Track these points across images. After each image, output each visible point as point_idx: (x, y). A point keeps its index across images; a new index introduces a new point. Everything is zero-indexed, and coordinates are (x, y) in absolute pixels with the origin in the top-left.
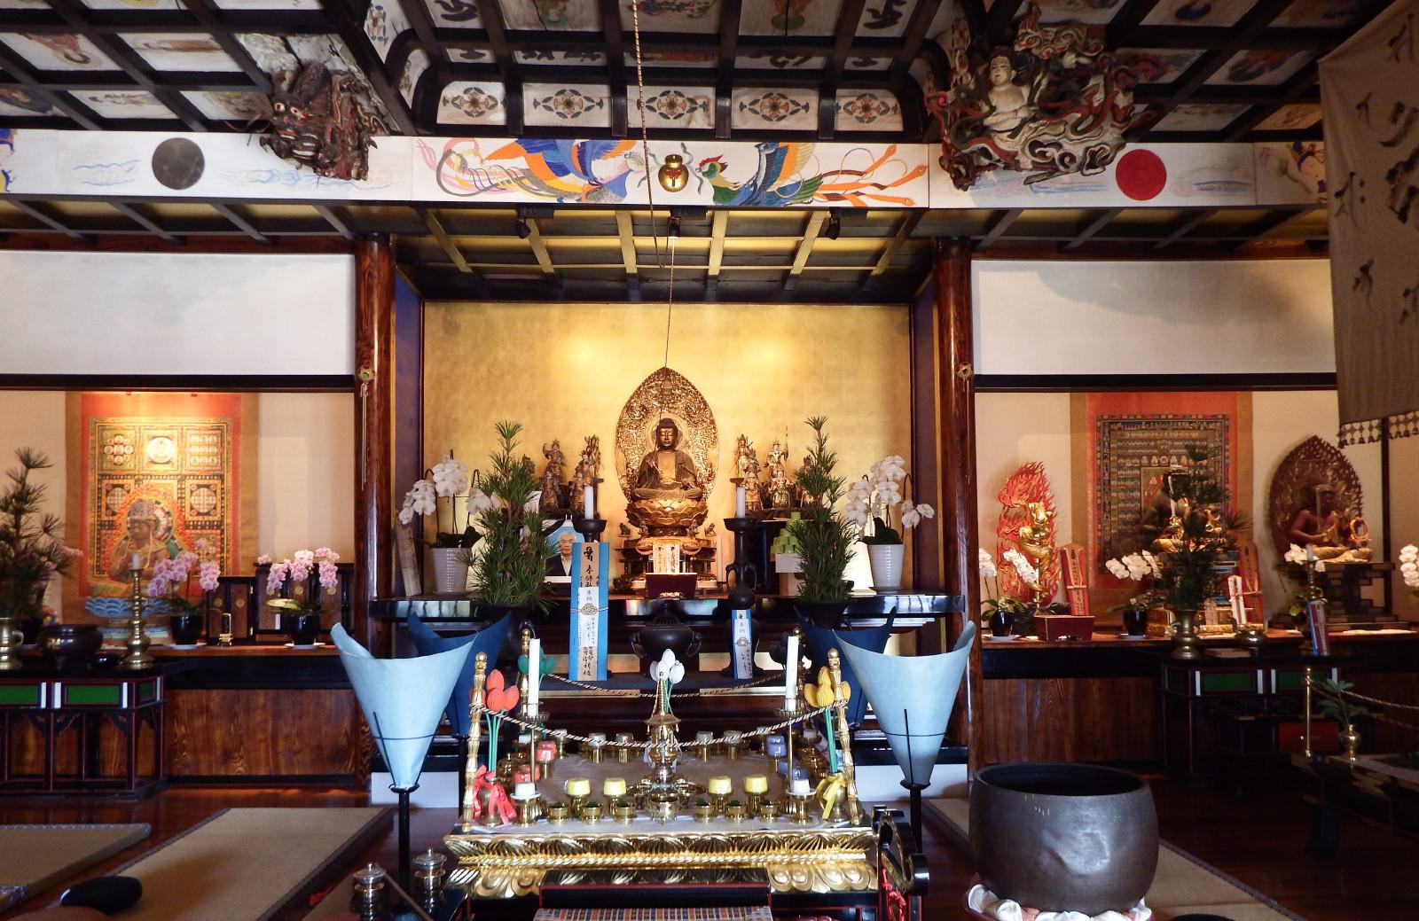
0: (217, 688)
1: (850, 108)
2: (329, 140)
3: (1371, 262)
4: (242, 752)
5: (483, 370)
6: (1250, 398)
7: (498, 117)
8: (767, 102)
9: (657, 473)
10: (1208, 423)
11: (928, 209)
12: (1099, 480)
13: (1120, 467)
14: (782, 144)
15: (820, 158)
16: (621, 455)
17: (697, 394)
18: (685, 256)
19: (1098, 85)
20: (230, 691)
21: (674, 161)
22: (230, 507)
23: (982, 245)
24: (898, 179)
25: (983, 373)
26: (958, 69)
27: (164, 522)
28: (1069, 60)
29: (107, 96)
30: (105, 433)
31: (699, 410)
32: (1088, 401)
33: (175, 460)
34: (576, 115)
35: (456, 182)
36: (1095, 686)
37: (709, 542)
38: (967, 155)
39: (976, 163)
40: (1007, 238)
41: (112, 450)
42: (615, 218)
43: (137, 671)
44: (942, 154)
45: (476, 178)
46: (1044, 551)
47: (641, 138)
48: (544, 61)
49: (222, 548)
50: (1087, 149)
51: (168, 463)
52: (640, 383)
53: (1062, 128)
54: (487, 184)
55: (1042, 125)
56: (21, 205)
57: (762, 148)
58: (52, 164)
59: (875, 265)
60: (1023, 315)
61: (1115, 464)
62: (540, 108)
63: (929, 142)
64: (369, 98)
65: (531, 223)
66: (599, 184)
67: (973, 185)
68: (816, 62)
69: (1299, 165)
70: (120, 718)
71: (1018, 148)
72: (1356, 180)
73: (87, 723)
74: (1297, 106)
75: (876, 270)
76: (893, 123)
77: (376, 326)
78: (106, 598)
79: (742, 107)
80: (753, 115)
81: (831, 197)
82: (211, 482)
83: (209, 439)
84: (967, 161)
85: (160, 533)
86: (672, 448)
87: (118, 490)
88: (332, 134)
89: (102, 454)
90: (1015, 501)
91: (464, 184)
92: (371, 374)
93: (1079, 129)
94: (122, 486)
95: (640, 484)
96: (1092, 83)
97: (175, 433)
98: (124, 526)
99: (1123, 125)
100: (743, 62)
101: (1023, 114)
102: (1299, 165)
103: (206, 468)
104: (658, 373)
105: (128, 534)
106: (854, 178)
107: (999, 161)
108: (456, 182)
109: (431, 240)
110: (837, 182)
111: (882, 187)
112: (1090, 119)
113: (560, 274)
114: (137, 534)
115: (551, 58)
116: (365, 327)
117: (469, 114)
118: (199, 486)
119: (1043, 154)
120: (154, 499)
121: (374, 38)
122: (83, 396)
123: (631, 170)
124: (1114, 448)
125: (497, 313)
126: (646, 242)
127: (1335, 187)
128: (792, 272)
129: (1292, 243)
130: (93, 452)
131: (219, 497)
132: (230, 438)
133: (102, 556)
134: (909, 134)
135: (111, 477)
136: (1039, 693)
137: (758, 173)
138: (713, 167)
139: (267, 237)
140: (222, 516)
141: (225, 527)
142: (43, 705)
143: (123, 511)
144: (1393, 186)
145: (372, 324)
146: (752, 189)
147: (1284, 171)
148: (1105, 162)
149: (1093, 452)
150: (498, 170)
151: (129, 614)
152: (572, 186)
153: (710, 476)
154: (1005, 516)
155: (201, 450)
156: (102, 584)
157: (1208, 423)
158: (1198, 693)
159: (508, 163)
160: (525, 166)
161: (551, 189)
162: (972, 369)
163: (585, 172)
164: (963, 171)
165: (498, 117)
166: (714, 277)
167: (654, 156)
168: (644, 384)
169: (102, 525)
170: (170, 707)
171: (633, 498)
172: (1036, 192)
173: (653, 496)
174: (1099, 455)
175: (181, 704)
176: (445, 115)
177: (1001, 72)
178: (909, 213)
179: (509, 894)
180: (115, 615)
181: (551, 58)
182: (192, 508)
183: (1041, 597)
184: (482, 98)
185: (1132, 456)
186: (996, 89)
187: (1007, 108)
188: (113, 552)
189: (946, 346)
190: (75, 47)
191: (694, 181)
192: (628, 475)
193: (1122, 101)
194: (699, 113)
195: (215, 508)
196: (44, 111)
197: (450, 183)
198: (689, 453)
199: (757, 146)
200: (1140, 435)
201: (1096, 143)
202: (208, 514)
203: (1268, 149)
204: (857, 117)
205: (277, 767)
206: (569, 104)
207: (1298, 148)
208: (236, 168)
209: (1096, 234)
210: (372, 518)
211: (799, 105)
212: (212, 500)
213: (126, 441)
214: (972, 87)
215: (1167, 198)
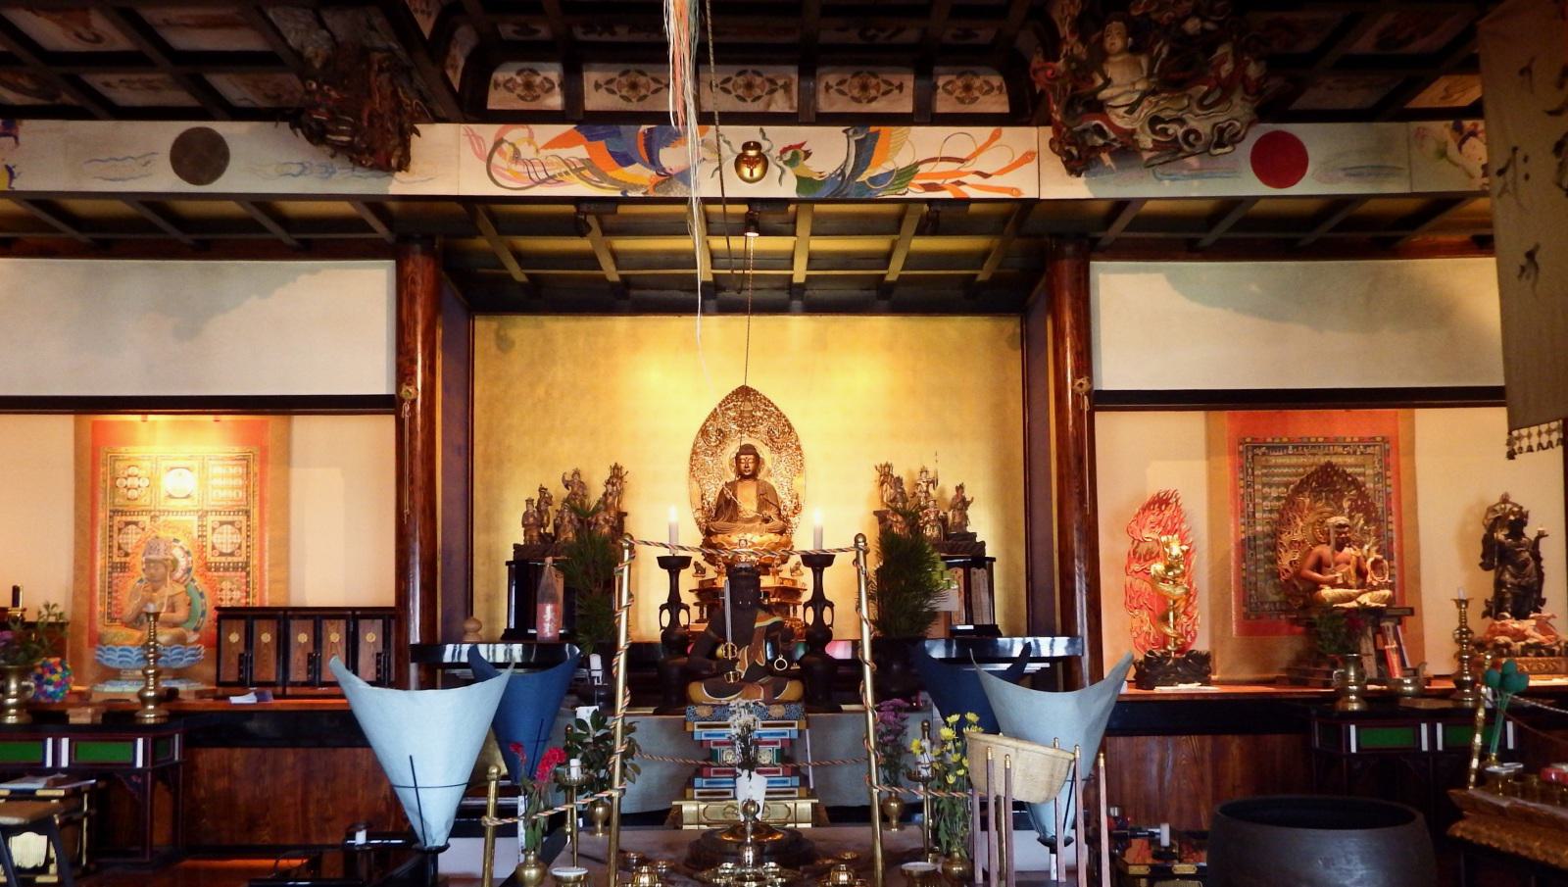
0: (242, 746)
1: (949, 87)
2: (366, 124)
3: (1537, 247)
4: (268, 818)
5: (541, 391)
6: (1413, 416)
7: (555, 101)
9: (735, 503)
10: (1365, 447)
11: (1037, 201)
13: (1265, 498)
14: (873, 129)
16: (695, 485)
17: (781, 416)
18: (766, 260)
19: (1226, 54)
20: (254, 750)
21: (752, 149)
22: (257, 546)
23: (1103, 243)
24: (1005, 166)
25: (1104, 389)
26: (1068, 39)
27: (183, 563)
28: (1192, 26)
29: (121, 81)
30: (117, 463)
31: (783, 434)
32: (1223, 418)
34: (642, 98)
35: (508, 174)
36: (1235, 745)
37: (794, 582)
39: (1090, 144)
40: (1131, 234)
41: (125, 483)
43: (150, 725)
44: (1052, 136)
45: (531, 169)
46: (1179, 591)
47: (714, 124)
48: (606, 37)
49: (248, 593)
50: (1215, 125)
51: (188, 497)
53: (1186, 102)
54: (543, 176)
55: (1164, 99)
57: (851, 133)
58: (57, 160)
59: (981, 268)
60: (1150, 322)
62: (603, 91)
63: (1038, 125)
64: (411, 80)
65: (592, 220)
68: (911, 35)
69: (1460, 149)
70: (134, 779)
71: (1137, 126)
72: (1520, 155)
74: (1458, 77)
76: (998, 104)
77: (419, 338)
78: (117, 645)
79: (828, 88)
80: (841, 97)
81: (928, 187)
82: (236, 518)
83: (233, 470)
84: (1077, 139)
85: (178, 575)
88: (370, 115)
89: (114, 487)
90: (1146, 534)
91: (516, 176)
93: (1206, 103)
94: (136, 523)
95: (717, 517)
96: (1220, 51)
97: (195, 464)
98: (140, 567)
100: (829, 36)
101: (1140, 86)
102: (1460, 149)
103: (230, 503)
105: (144, 576)
106: (954, 166)
107: (1114, 140)
108: (508, 174)
109: (481, 243)
110: (935, 171)
111: (985, 176)
112: (1217, 94)
114: (152, 576)
115: (613, 33)
116: (407, 339)
117: (522, 98)
118: (222, 523)
119: (1164, 131)
120: (171, 536)
121: (416, 10)
122: (95, 423)
124: (1258, 476)
126: (719, 243)
127: (1496, 167)
129: (1457, 238)
130: (103, 484)
132: (256, 469)
133: (114, 602)
134: (1016, 117)
135: (123, 513)
137: (846, 161)
138: (795, 156)
139: (297, 240)
140: (248, 557)
143: (137, 550)
144: (1560, 160)
145: (415, 335)
146: (840, 179)
147: (1443, 154)
148: (1235, 140)
150: (555, 160)
151: (143, 665)
152: (638, 177)
154: (1135, 552)
155: (225, 482)
156: (113, 630)
157: (1365, 447)
158: (1354, 750)
159: (565, 153)
160: (585, 155)
161: (614, 182)
163: (653, 161)
164: (1075, 152)
165: (555, 101)
167: (728, 143)
169: (113, 567)
170: (189, 764)
171: (708, 533)
174: (1242, 483)
175: (200, 766)
176: (496, 100)
177: (1115, 39)
180: (128, 666)
181: (613, 33)
182: (214, 548)
183: (1176, 644)
184: (538, 80)
186: (1112, 59)
187: (1122, 86)
188: (128, 595)
189: (1061, 365)
190: (87, 25)
191: (774, 171)
192: (703, 508)
193: (1253, 70)
194: (779, 95)
195: (240, 548)
197: (503, 176)
198: (772, 481)
199: (845, 131)
200: (1287, 460)
201: (1225, 118)
202: (232, 554)
203: (1424, 129)
204: (958, 98)
205: (307, 835)
206: (634, 86)
207: (1458, 128)
208: (263, 164)
210: (414, 553)
211: (890, 84)
212: (238, 539)
213: (142, 473)
214: (1084, 57)
215: (1309, 186)
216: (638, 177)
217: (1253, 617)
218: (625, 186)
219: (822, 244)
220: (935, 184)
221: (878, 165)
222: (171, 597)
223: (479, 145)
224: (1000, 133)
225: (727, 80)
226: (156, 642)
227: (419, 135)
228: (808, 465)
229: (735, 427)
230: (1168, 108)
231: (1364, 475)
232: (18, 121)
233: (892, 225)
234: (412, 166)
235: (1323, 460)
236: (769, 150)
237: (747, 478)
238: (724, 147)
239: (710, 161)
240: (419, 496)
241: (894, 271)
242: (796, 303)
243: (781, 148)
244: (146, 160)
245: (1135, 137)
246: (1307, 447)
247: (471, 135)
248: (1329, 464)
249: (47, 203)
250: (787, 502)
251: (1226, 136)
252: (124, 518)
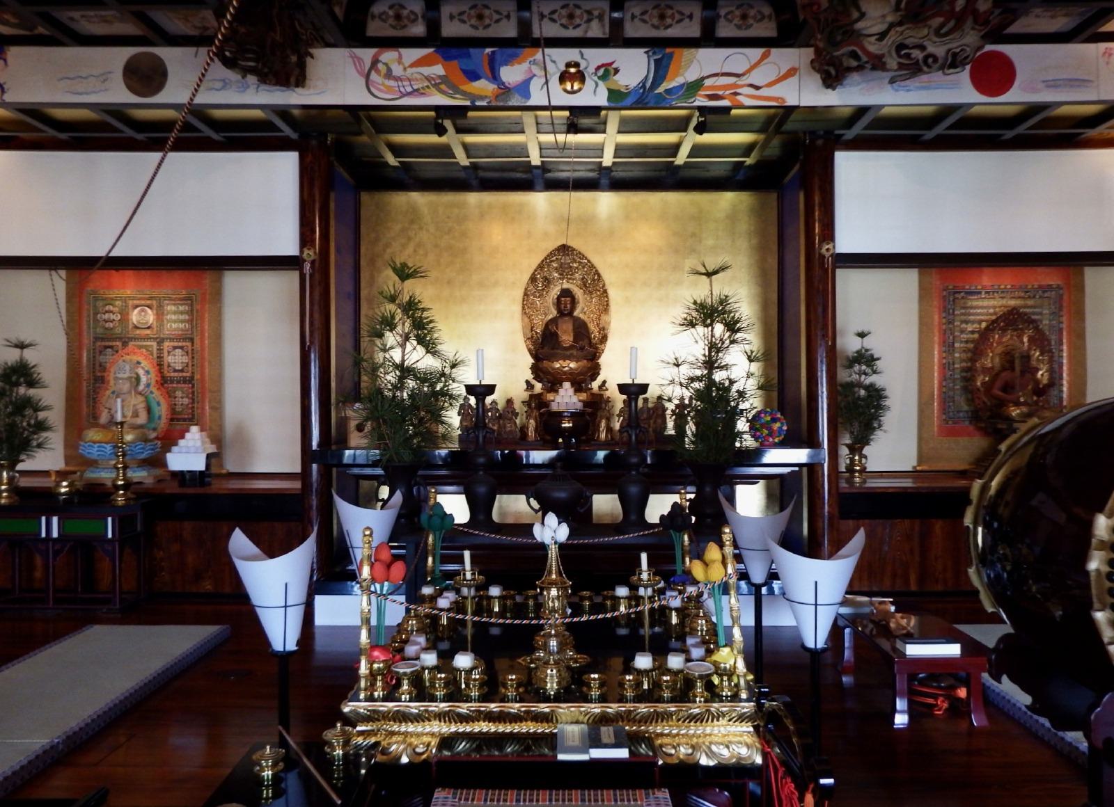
1: (729, 17)
7: (419, 30)
8: (655, 12)
10: (1044, 292)
11: (797, 107)
12: (944, 342)
13: (962, 331)
14: (668, 50)
15: (702, 63)
16: (526, 320)
24: (778, 80)
29: (83, 16)
32: (934, 277)
33: (155, 326)
38: (837, 57)
39: (845, 64)
42: (521, 117)
49: (193, 399)
50: (949, 50)
52: (542, 258)
54: (409, 89)
55: (908, 29)
56: (17, 113)
57: (650, 54)
59: (748, 156)
60: (875, 201)
61: (957, 329)
63: (800, 46)
65: (448, 124)
66: (507, 88)
67: (841, 84)
71: (885, 51)
73: (79, 548)
75: (749, 161)
76: (767, 29)
79: (633, 17)
80: (643, 24)
82: (184, 344)
87: (109, 350)
91: (389, 89)
92: (309, 254)
93: (943, 31)
94: (111, 347)
99: (982, 28)
101: (890, 19)
103: (180, 332)
106: (732, 80)
107: (867, 62)
109: (364, 139)
110: (717, 84)
111: (757, 88)
112: (952, 23)
113: (474, 167)
117: (394, 27)
118: (175, 348)
119: (908, 56)
123: (534, 75)
124: (958, 315)
126: (548, 138)
128: (676, 163)
131: (190, 356)
134: (785, 38)
136: (887, 531)
137: (646, 77)
139: (224, 137)
140: (193, 373)
141: (195, 382)
142: (44, 535)
145: (314, 211)
146: (641, 91)
149: (939, 318)
153: (603, 338)
159: (427, 71)
161: (466, 95)
162: (834, 247)
163: (495, 77)
164: (833, 72)
165: (419, 30)
166: (607, 168)
168: (546, 258)
172: (897, 90)
174: (944, 321)
176: (374, 29)
178: (781, 111)
179: (405, 760)
180: (103, 458)
184: (405, 13)
185: (973, 322)
191: (589, 83)
192: (532, 337)
194: (595, 24)
195: (187, 366)
196: (31, 30)
199: (646, 52)
202: (182, 371)
204: (736, 25)
206: (480, 17)
209: (865, 128)
211: (681, 13)
212: (185, 359)
213: (116, 309)
216: (484, 87)
217: (950, 422)
218: (473, 98)
220: (717, 95)
221: (673, 79)
222: (134, 406)
223: (360, 64)
224: (769, 54)
225: (554, 12)
226: (122, 443)
227: (312, 57)
229: (556, 275)
230: (911, 37)
231: (1041, 314)
232: (6, 48)
234: (307, 82)
236: (586, 68)
237: (566, 315)
238: (550, 66)
239: (540, 77)
241: (681, 158)
243: (596, 66)
244: (104, 77)
245: (884, 60)
246: (997, 292)
247: (354, 57)
249: (35, 112)
251: (959, 59)
252: (103, 344)
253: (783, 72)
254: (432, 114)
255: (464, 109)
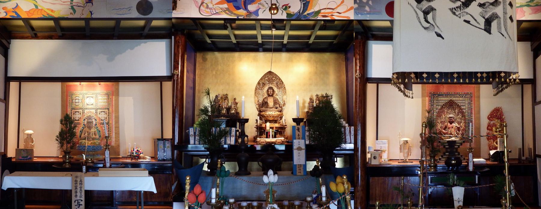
5: (214, 73)
16: (256, 98)
17: (280, 79)
18: (277, 37)
31: (280, 84)
54: (215, 12)
65: (228, 25)
67: (316, 73)
75: (335, 42)
81: (323, 16)
86: (272, 96)
104: (268, 73)
106: (331, 11)
111: (340, 13)
118: (78, 120)
125: (218, 55)
126: (264, 32)
135: (75, 109)
152: (242, 13)
159: (221, 6)
160: (227, 7)
161: (235, 14)
163: (246, 9)
173: (266, 111)
191: (280, 11)
198: (277, 97)
212: (106, 116)
216: (242, 13)
218: (238, 16)
219: (292, 33)
228: (287, 91)
233: (312, 27)
235: (449, 99)
240: (179, 101)
242: (284, 49)
248: (451, 100)
250: (282, 103)
253: (349, 8)
254: (223, 22)
255: (234, 20)
